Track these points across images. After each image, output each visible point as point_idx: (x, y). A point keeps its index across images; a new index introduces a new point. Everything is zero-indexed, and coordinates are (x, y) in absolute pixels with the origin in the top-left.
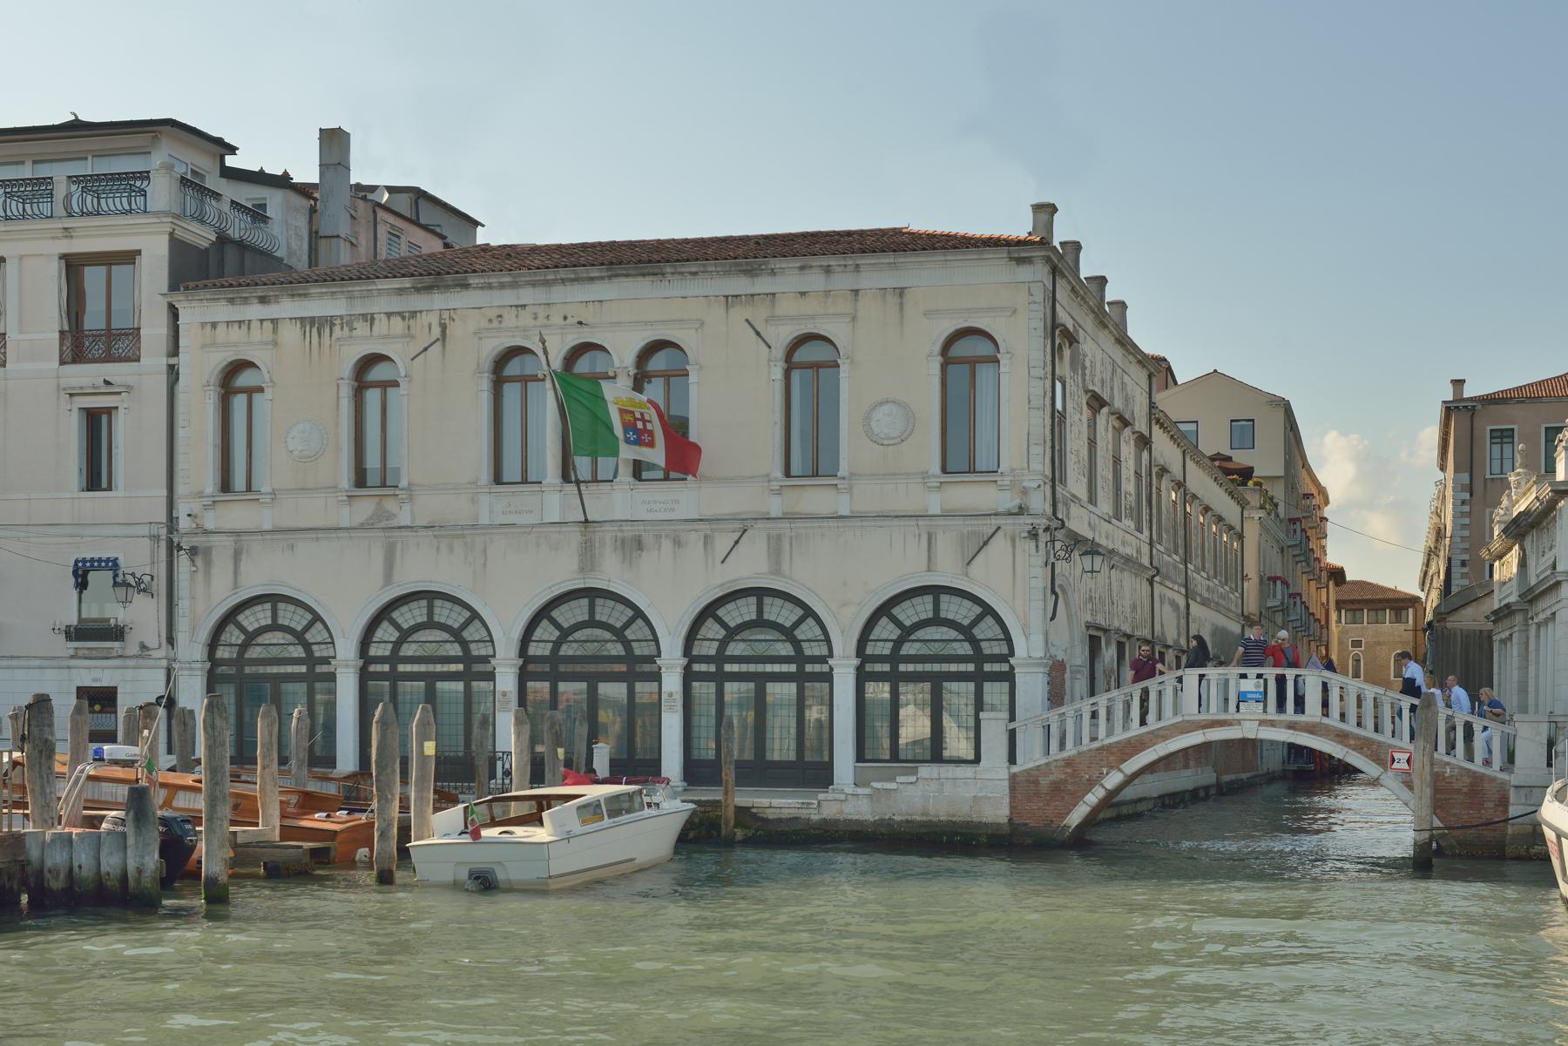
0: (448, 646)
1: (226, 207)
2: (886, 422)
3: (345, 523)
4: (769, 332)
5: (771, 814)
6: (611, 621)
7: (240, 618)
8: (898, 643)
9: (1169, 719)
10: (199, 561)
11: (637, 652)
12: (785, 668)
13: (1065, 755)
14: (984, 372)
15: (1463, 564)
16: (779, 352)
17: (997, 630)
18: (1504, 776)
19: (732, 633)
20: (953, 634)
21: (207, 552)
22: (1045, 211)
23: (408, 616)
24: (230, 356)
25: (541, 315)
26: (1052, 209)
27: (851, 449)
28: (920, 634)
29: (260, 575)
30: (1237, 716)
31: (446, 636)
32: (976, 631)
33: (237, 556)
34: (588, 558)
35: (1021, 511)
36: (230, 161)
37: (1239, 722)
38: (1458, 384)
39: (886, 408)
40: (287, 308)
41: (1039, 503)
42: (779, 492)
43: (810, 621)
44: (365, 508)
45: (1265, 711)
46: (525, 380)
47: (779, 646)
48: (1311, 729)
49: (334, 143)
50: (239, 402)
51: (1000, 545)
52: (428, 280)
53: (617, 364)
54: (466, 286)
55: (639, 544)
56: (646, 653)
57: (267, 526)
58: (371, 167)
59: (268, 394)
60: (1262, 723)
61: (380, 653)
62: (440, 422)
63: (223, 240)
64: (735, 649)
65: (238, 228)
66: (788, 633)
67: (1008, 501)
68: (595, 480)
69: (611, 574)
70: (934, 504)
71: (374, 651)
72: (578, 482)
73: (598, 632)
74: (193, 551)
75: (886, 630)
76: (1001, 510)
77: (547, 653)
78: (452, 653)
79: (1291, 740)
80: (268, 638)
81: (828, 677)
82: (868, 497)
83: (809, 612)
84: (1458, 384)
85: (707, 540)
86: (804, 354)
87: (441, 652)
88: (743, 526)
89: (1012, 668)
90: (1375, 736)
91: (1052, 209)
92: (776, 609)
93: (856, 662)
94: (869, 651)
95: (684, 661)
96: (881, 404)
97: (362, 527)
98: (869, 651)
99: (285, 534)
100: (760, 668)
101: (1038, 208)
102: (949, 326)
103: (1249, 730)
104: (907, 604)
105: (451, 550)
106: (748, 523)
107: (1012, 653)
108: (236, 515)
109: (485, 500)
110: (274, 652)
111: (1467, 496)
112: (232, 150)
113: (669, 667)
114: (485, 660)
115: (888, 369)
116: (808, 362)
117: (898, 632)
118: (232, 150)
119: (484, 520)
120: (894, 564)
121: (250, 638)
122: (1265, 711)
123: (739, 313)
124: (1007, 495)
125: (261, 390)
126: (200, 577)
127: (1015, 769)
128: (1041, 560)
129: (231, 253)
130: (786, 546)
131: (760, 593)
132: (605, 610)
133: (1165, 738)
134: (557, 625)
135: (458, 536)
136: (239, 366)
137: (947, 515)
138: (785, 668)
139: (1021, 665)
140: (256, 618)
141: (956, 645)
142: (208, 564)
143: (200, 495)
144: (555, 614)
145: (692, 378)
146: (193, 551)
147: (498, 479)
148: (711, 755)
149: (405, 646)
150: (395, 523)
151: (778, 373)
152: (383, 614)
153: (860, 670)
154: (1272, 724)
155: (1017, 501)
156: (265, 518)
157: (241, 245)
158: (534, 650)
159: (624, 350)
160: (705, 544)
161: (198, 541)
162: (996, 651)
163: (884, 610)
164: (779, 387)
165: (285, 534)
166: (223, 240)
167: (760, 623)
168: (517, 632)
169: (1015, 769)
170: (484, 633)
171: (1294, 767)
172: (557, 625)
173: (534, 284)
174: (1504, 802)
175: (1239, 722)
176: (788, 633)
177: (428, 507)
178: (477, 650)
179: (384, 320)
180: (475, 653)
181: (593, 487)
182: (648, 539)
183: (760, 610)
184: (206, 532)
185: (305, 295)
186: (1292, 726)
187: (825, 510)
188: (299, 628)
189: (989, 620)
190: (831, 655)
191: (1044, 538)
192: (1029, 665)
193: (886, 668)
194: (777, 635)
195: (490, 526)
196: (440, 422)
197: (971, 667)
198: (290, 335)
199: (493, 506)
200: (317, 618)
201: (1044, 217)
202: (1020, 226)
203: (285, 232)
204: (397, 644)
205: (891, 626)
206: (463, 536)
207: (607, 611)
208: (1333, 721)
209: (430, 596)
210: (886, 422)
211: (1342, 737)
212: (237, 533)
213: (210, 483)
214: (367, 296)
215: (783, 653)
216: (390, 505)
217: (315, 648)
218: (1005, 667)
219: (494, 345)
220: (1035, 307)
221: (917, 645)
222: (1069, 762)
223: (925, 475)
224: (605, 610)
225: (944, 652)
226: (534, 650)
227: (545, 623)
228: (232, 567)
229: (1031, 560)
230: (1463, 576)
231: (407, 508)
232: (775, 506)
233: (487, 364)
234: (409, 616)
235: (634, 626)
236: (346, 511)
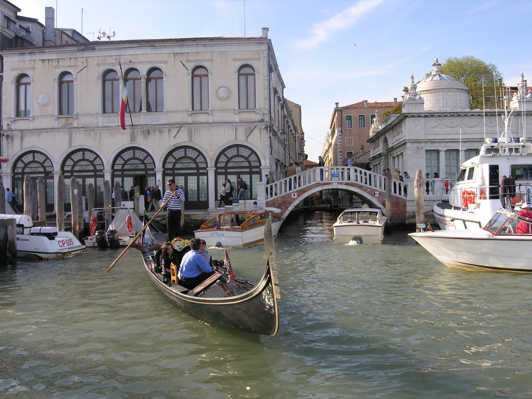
0: (89, 166)
1: (18, 27)
2: (222, 93)
3: (56, 126)
4: (187, 65)
5: (194, 218)
6: (140, 158)
7: (23, 159)
8: (227, 163)
9: (312, 183)
10: (10, 140)
11: (148, 167)
12: (193, 171)
13: (282, 195)
14: (250, 78)
15: (340, 152)
16: (190, 71)
17: (256, 158)
18: (405, 198)
19: (177, 161)
20: (243, 160)
21: (12, 138)
22: (266, 29)
23: (77, 157)
24: (20, 72)
25: (118, 59)
26: (268, 29)
27: (213, 103)
28: (233, 160)
29: (30, 143)
30: (331, 182)
31: (88, 163)
32: (249, 159)
33: (22, 138)
34: (133, 138)
35: (262, 121)
36: (19, 14)
37: (332, 183)
38: (337, 104)
39: (222, 89)
40: (38, 57)
41: (267, 118)
42: (191, 115)
43: (201, 156)
44: (63, 122)
45: (339, 179)
46: (113, 80)
47: (191, 164)
48: (352, 185)
49: (50, 12)
50: (22, 88)
51: (256, 132)
52: (83, 47)
53: (141, 74)
54: (94, 49)
55: (149, 132)
56: (151, 167)
57: (32, 128)
58: (60, 23)
59: (32, 85)
60: (338, 183)
61: (68, 169)
62: (87, 95)
63: (17, 37)
64: (178, 166)
65: (23, 33)
66: (194, 160)
67: (258, 117)
68: (134, 112)
69: (140, 142)
70: (237, 119)
71: (66, 169)
72: (130, 112)
73: (136, 161)
74: (8, 136)
75: (223, 159)
76: (257, 120)
77: (120, 168)
78: (90, 169)
79: (347, 188)
80: (32, 165)
81: (206, 174)
82: (217, 117)
83: (200, 153)
84: (337, 104)
85: (169, 131)
86: (198, 72)
87: (87, 169)
88: (180, 126)
89: (261, 170)
90: (370, 186)
91: (267, 29)
92: (190, 153)
93: (215, 169)
94: (218, 165)
95: (162, 170)
96: (221, 87)
97: (62, 128)
98: (218, 165)
99: (39, 131)
100: (186, 172)
101: (264, 29)
102: (240, 63)
103: (335, 186)
104: (229, 150)
105: (90, 135)
106: (182, 125)
107: (260, 165)
108: (21, 125)
109: (101, 118)
110: (34, 170)
111: (341, 134)
112: (19, 10)
113: (158, 171)
114: (101, 171)
115: (223, 77)
116: (199, 73)
117: (227, 159)
118: (19, 10)
119: (101, 125)
120: (223, 138)
121: (26, 165)
122: (339, 179)
123: (179, 58)
124: (258, 116)
125: (29, 84)
126: (10, 145)
127: (267, 200)
128: (268, 136)
129: (19, 41)
130: (193, 131)
131: (186, 147)
132: (138, 154)
133: (311, 189)
134: (123, 159)
135: (92, 130)
136: (23, 76)
137: (241, 122)
138: (193, 171)
139: (264, 169)
140: (28, 159)
141: (244, 163)
142: (12, 140)
143: (10, 118)
144: (122, 155)
145: (164, 79)
146: (8, 136)
147: (104, 112)
148: (21, 204)
149: (76, 167)
150: (72, 126)
151: (190, 78)
152: (69, 156)
153: (216, 171)
154: (341, 183)
155: (262, 117)
156: (31, 125)
157: (22, 39)
158: (116, 167)
159: (143, 70)
160: (169, 132)
161: (9, 133)
162: (256, 165)
163: (222, 152)
164: (190, 82)
165: (39, 131)
166: (17, 37)
167: (186, 157)
168: (111, 162)
169: (267, 200)
170: (100, 162)
171: (305, 207)
172: (123, 159)
173: (115, 49)
174: (405, 206)
175: (332, 183)
176: (194, 160)
177: (83, 121)
178: (98, 168)
179: (69, 60)
180: (98, 169)
181: (134, 114)
182: (151, 130)
183: (185, 153)
184: (12, 130)
185: (43, 52)
186: (346, 184)
187: (205, 121)
188: (194, 157)
189: (253, 155)
190: (207, 167)
191: (268, 129)
192: (266, 169)
193: (223, 171)
194: (191, 161)
195: (102, 127)
196: (87, 95)
197: (248, 170)
198: (39, 64)
199: (102, 121)
200: (47, 158)
201: (265, 32)
202: (259, 34)
203: (36, 36)
204: (73, 167)
205: (225, 157)
206: (94, 130)
207: (139, 154)
208: (359, 182)
209: (83, 150)
210: (222, 93)
211: (360, 187)
212: (22, 130)
213: (13, 114)
214: (63, 52)
215: (193, 167)
216: (71, 120)
217: (47, 168)
218: (258, 170)
219: (103, 69)
220: (265, 58)
221: (232, 163)
222: (283, 197)
223: (234, 110)
224: (138, 154)
225: (189, 167)
226: (116, 167)
227: (119, 158)
228: (20, 142)
229: (266, 135)
230: (340, 155)
231: (76, 121)
232: (190, 120)
233: (101, 75)
234: (77, 157)
235: (147, 159)
236: (57, 122)
